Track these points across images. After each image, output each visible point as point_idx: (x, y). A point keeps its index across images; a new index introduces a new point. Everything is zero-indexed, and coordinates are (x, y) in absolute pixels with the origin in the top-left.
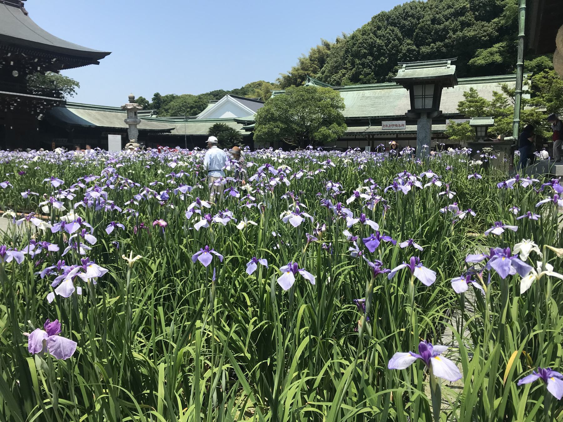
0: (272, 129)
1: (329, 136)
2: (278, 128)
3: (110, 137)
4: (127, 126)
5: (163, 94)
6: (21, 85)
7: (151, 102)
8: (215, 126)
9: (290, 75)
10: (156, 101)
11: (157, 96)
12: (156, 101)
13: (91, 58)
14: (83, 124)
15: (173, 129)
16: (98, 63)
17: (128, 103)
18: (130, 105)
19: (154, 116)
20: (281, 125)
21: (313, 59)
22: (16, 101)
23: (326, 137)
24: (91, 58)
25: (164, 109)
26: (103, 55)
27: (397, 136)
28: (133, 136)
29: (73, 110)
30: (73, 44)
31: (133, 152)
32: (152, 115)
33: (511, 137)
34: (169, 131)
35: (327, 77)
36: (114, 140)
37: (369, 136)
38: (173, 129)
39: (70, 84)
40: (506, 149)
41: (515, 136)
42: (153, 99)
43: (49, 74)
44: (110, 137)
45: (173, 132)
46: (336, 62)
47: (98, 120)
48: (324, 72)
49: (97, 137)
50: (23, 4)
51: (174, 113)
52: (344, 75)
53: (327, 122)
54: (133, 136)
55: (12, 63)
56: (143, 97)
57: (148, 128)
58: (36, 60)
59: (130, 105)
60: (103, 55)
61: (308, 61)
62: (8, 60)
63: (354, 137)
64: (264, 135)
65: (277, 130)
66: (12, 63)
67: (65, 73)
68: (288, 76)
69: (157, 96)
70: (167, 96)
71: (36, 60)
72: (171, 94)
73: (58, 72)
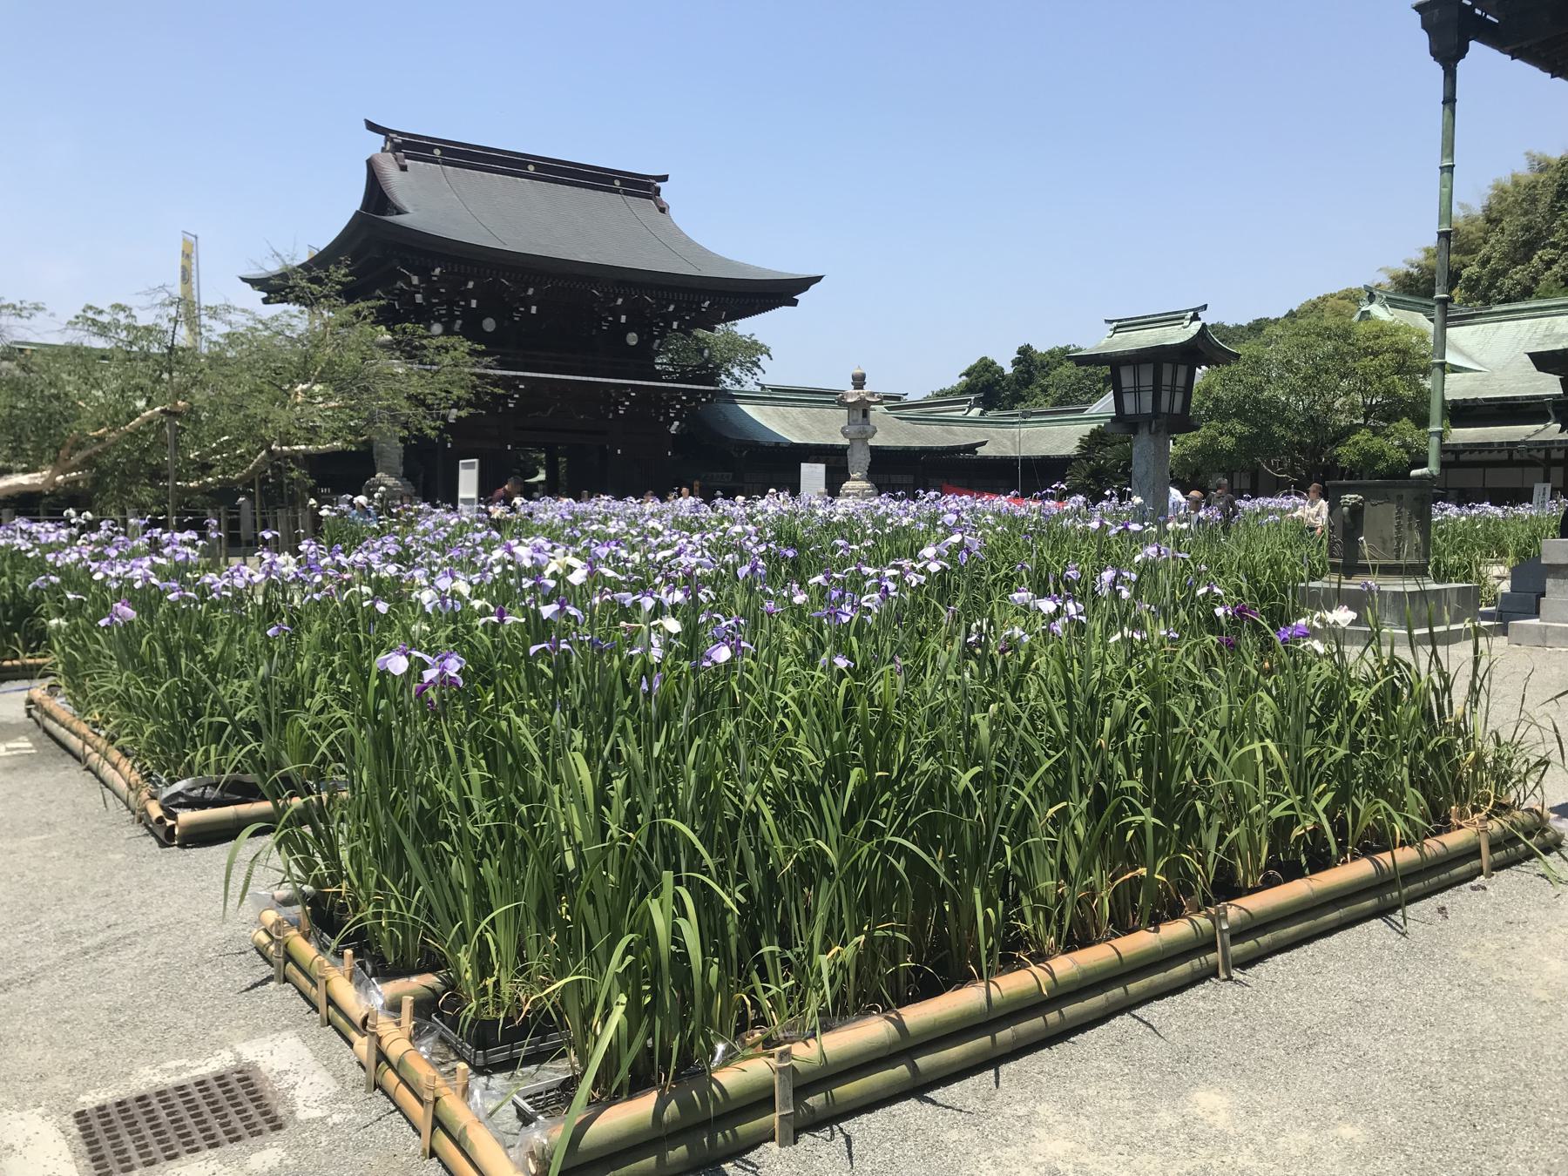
0: (1214, 439)
1: (1381, 456)
2: (1232, 435)
3: (805, 468)
4: (846, 442)
5: (1041, 347)
6: (641, 363)
7: (1009, 370)
8: (1093, 432)
9: (1415, 271)
10: (1021, 367)
11: (1025, 353)
12: (1021, 367)
13: (780, 293)
14: (763, 439)
15: (984, 443)
16: (795, 303)
17: (850, 389)
18: (852, 395)
19: (976, 411)
20: (1238, 427)
21: (1494, 215)
22: (628, 397)
23: (1370, 458)
24: (780, 293)
25: (1041, 386)
26: (805, 283)
27: (1511, 455)
28: (859, 461)
29: (749, 409)
30: (745, 267)
31: (857, 497)
32: (970, 408)
33: (1425, 470)
34: (971, 448)
35: (1496, 274)
36: (813, 475)
37: (1548, 452)
38: (984, 443)
39: (753, 352)
40: (1401, 497)
41: (1432, 468)
42: (1015, 363)
43: (701, 333)
44: (805, 468)
45: (982, 451)
46: (1527, 228)
47: (802, 428)
48: (1488, 260)
49: (775, 465)
50: (658, 190)
51: (1060, 398)
52: (1549, 264)
53: (1391, 411)
54: (859, 461)
55: (623, 319)
56: (990, 358)
57: (916, 443)
58: (671, 308)
59: (852, 395)
60: (805, 283)
61: (1481, 223)
62: (616, 313)
63: (1505, 456)
64: (1192, 456)
65: (1227, 442)
66: (623, 319)
67: (745, 327)
68: (1408, 275)
69: (1025, 353)
70: (1051, 353)
71: (671, 308)
72: (1063, 345)
73: (712, 330)
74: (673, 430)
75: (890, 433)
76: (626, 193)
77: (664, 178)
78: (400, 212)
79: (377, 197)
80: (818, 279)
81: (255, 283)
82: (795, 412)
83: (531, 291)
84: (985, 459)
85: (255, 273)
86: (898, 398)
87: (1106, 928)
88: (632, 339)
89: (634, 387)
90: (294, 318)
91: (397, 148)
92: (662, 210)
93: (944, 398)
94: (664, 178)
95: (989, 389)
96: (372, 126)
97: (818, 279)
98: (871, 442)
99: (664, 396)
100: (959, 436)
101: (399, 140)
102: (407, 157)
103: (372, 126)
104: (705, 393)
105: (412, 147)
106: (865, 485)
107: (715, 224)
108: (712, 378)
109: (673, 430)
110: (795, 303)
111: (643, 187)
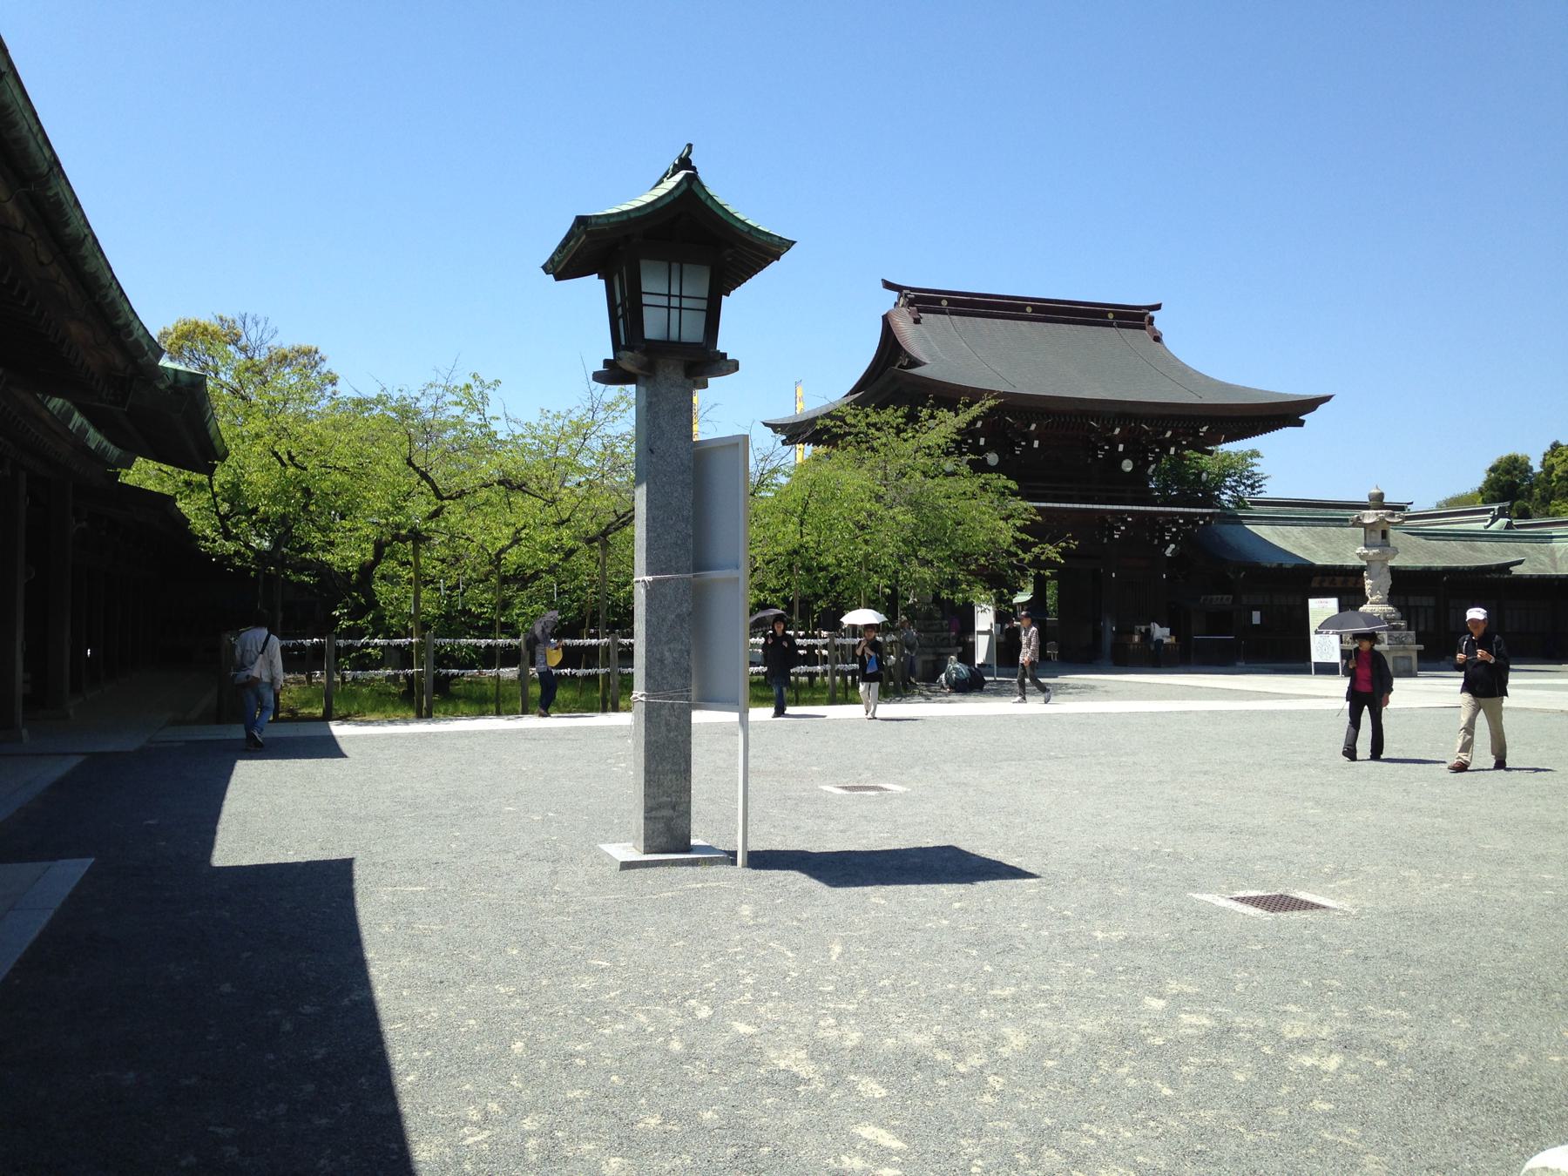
14: (1271, 561)
15: (1520, 562)
16: (1301, 424)
26: (1312, 404)
32: (1494, 519)
34: (1505, 568)
38: (1520, 562)
50: (1152, 319)
57: (1438, 563)
58: (1169, 434)
60: (1312, 404)
66: (1121, 448)
71: (1169, 434)
74: (1168, 553)
75: (1413, 555)
76: (1120, 326)
77: (1157, 307)
78: (915, 363)
79: (890, 344)
80: (1326, 399)
81: (775, 427)
82: (1296, 530)
83: (1033, 427)
84: (1520, 578)
85: (768, 419)
86: (1402, 508)
87: (498, 652)
88: (1127, 466)
89: (1131, 513)
90: (851, 477)
91: (911, 303)
92: (1157, 339)
93: (1457, 507)
94: (1157, 307)
95: (1511, 488)
96: (888, 285)
97: (1326, 399)
98: (1391, 563)
99: (1161, 520)
100: (1488, 555)
101: (912, 295)
102: (919, 311)
103: (888, 285)
104: (1203, 516)
105: (924, 302)
106: (1388, 608)
107: (1213, 348)
108: (1210, 500)
109: (1168, 553)
110: (1301, 424)
111: (1135, 318)
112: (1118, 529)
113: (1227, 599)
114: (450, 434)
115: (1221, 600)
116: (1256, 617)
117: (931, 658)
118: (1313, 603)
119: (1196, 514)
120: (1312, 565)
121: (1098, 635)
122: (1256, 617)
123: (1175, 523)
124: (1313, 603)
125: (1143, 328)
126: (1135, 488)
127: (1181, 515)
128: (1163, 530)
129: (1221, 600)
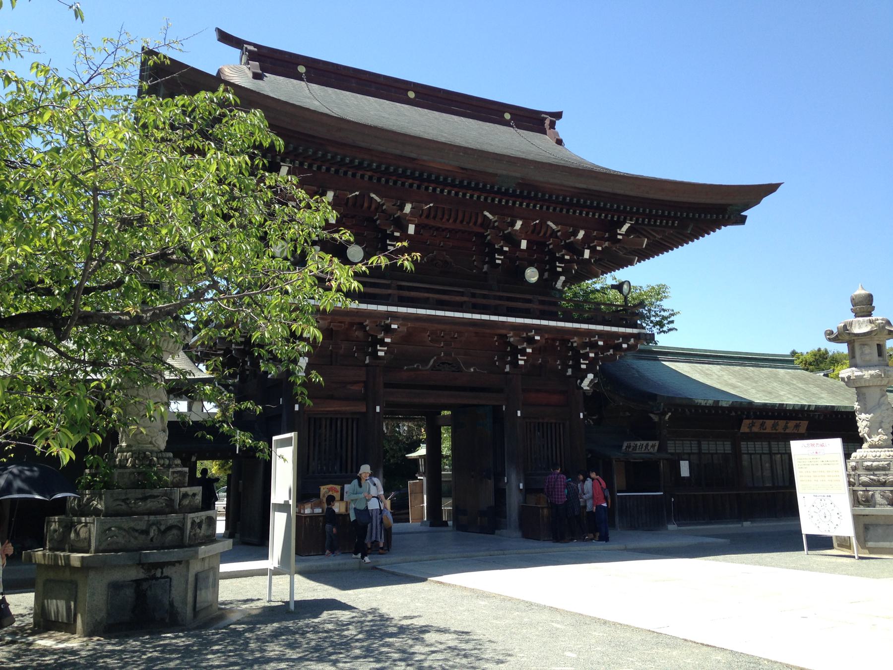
16: (742, 220)
26: (756, 194)
58: (581, 234)
71: (581, 234)
74: (585, 385)
80: (771, 189)
82: (715, 369)
88: (532, 275)
89: (539, 329)
97: (771, 189)
109: (585, 385)
112: (523, 352)
113: (652, 446)
114: (581, 477)
115: (646, 447)
116: (685, 469)
117: (134, 574)
118: (322, 488)
119: (617, 335)
120: (751, 403)
121: (500, 494)
122: (685, 469)
123: (593, 346)
124: (322, 488)
125: (544, 132)
126: (544, 300)
127: (601, 334)
128: (577, 356)
129: (646, 447)
